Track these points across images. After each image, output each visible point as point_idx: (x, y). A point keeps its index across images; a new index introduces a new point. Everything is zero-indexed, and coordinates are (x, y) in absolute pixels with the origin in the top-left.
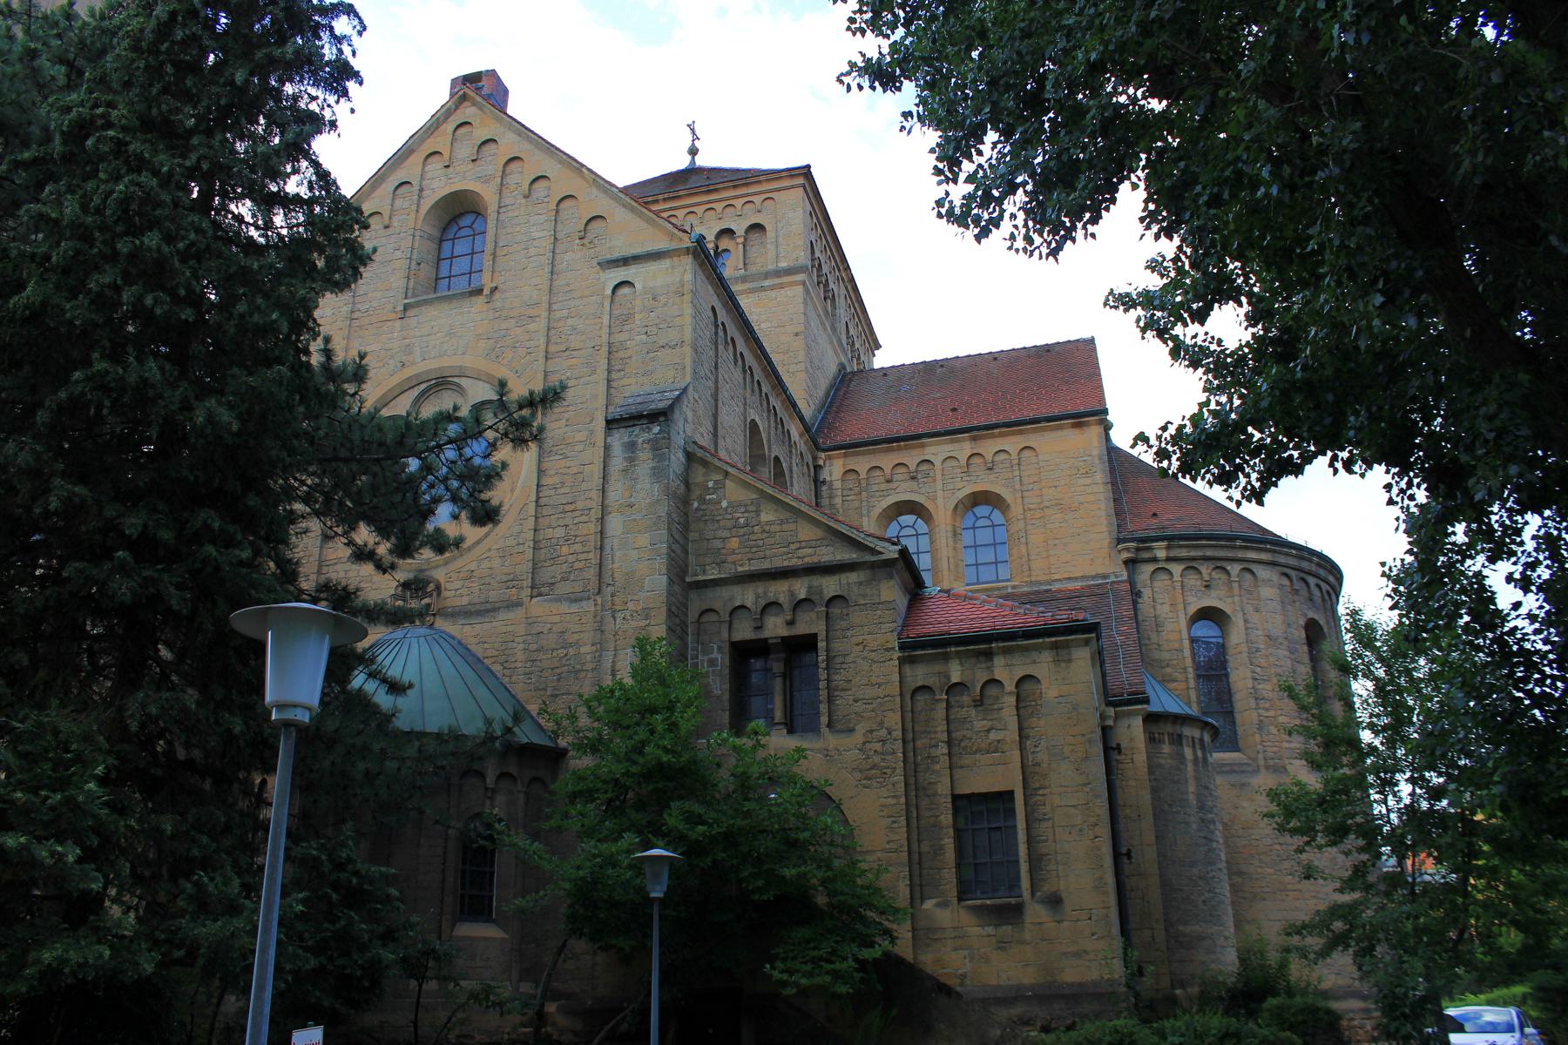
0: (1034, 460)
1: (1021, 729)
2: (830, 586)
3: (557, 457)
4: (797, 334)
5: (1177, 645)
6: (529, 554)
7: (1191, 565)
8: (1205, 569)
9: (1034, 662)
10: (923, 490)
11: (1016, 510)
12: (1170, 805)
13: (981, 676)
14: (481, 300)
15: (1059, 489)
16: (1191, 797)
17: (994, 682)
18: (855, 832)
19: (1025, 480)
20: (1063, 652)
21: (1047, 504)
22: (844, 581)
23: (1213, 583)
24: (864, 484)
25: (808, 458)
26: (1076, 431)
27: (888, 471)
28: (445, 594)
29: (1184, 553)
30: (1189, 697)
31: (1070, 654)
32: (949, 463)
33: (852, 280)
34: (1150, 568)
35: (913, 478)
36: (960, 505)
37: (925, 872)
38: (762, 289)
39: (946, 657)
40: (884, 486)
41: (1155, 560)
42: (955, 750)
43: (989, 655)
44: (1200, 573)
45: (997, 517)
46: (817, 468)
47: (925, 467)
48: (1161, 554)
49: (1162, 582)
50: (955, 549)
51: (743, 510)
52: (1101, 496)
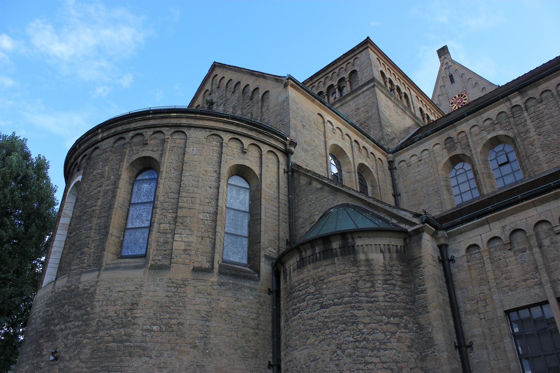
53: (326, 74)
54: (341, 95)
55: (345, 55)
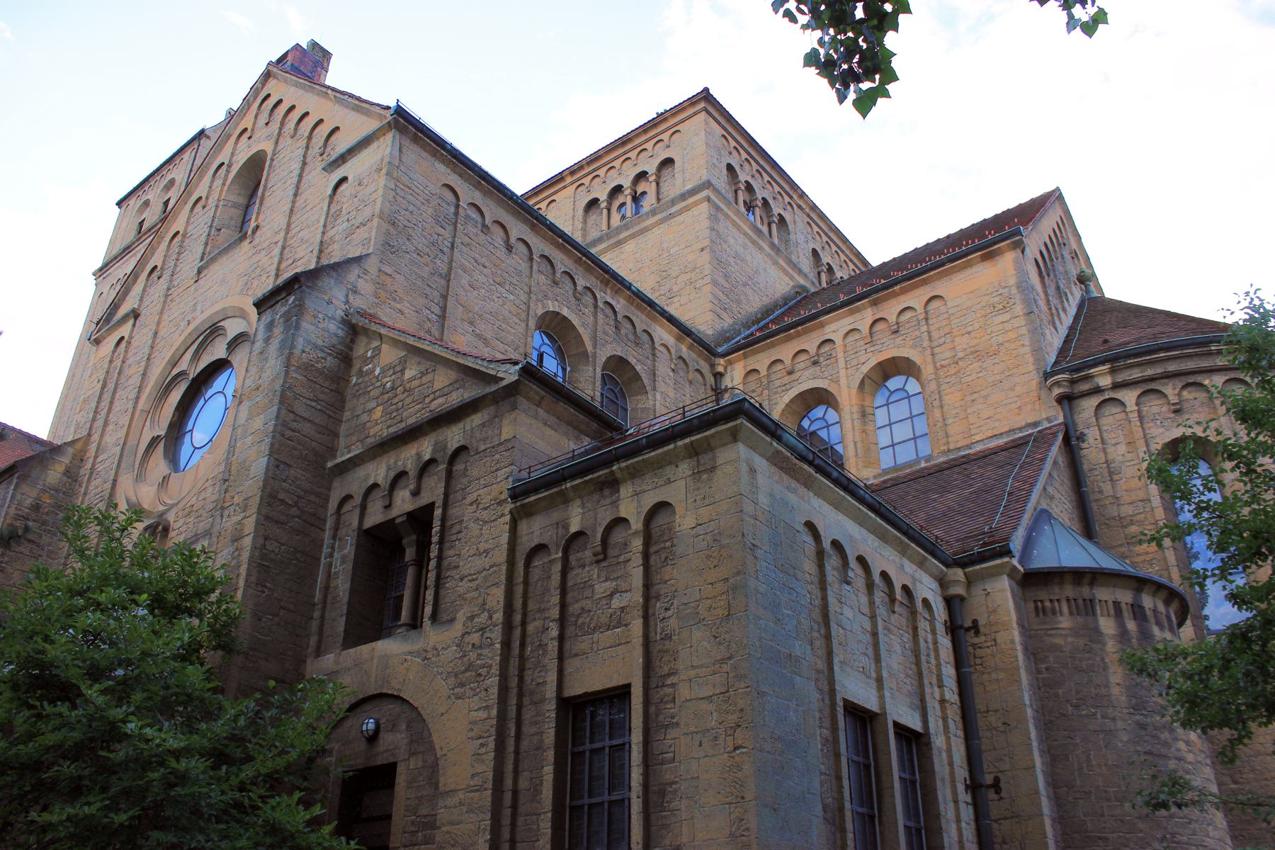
0: (943, 309)
1: (647, 585)
2: (454, 436)
4: (702, 250)
5: (1141, 495)
7: (1149, 388)
8: (1170, 389)
9: (669, 482)
10: (826, 374)
11: (927, 371)
12: (1077, 707)
13: (605, 517)
15: (973, 334)
16: (1116, 691)
17: (620, 521)
18: (441, 763)
19: (935, 335)
20: (704, 459)
21: (960, 355)
22: (468, 427)
23: (1185, 405)
24: (765, 381)
25: (705, 368)
26: (987, 264)
27: (788, 361)
28: (172, 534)
29: (1136, 374)
30: (1165, 559)
31: (714, 459)
32: (850, 338)
33: (814, 207)
34: (1094, 401)
35: (815, 363)
36: (867, 382)
37: (520, 820)
38: (672, 216)
39: (565, 499)
40: (787, 379)
41: (1098, 390)
42: (570, 631)
43: (613, 484)
44: (1165, 396)
45: (913, 386)
46: (718, 376)
47: (826, 348)
48: (1105, 381)
49: (1111, 416)
50: (864, 431)
51: (391, 372)
52: (1024, 331)
53: (625, 153)
54: (637, 212)
55: (595, 158)
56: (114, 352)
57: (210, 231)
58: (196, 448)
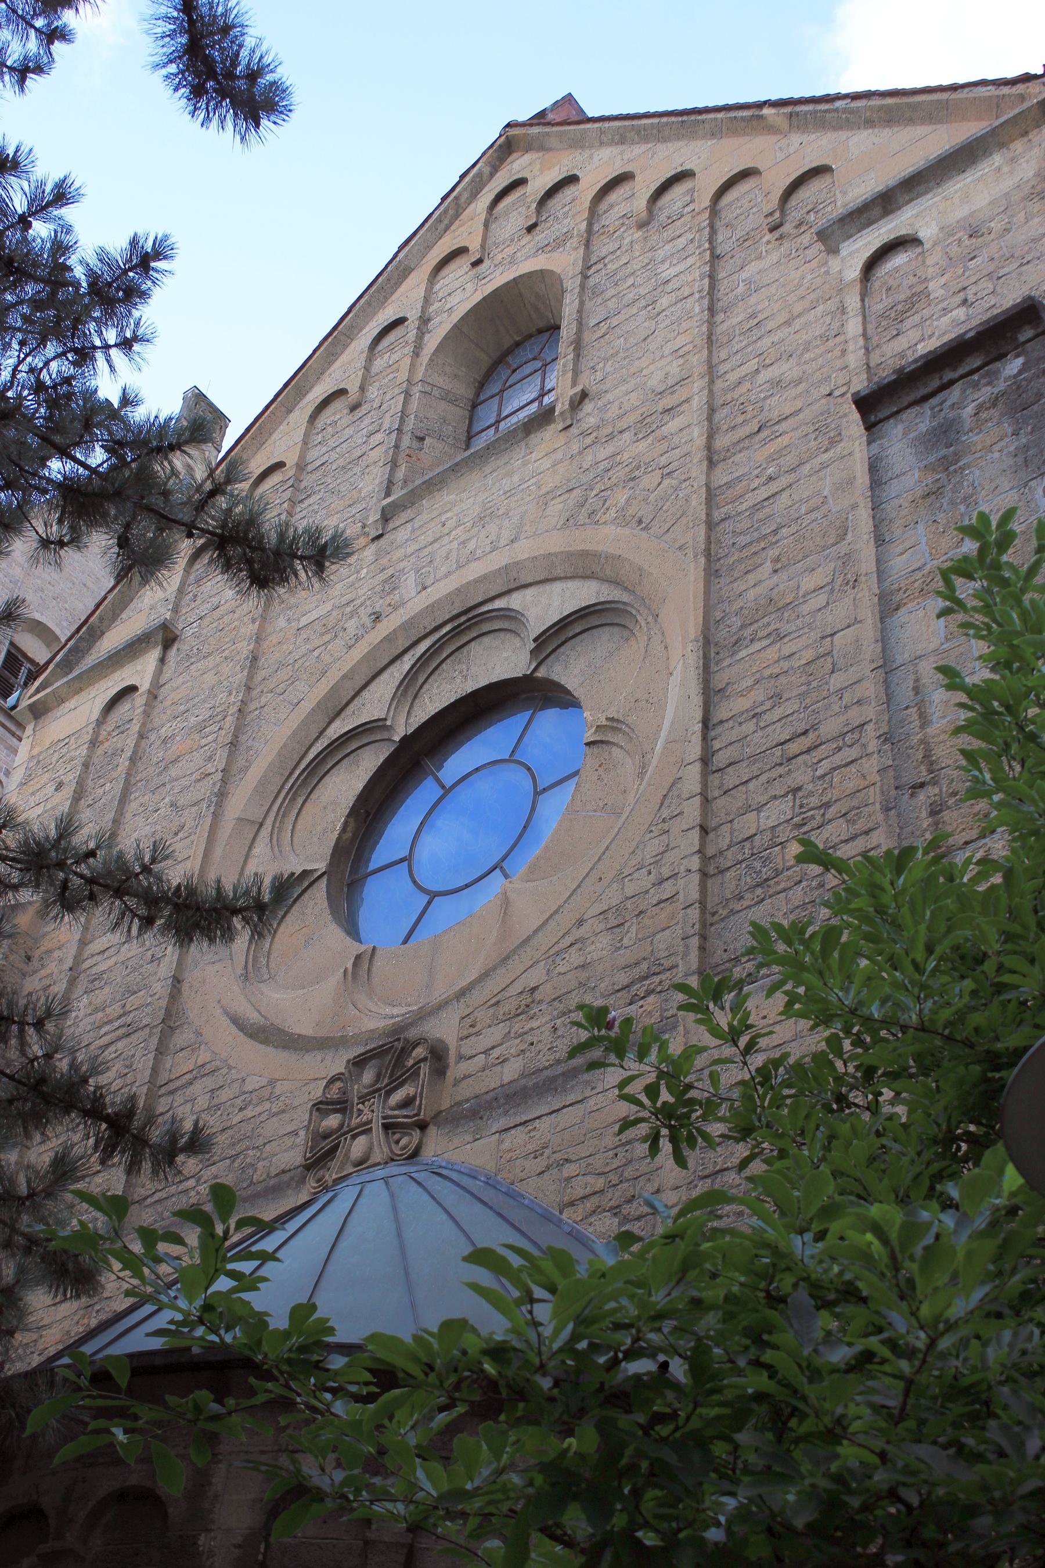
3: (758, 646)
6: (690, 888)
14: (549, 436)
28: (456, 1070)
56: (100, 722)
57: (398, 440)
58: (433, 895)
